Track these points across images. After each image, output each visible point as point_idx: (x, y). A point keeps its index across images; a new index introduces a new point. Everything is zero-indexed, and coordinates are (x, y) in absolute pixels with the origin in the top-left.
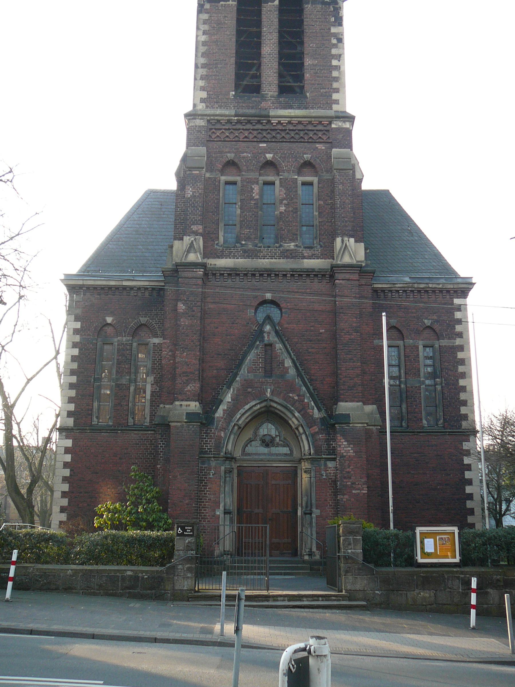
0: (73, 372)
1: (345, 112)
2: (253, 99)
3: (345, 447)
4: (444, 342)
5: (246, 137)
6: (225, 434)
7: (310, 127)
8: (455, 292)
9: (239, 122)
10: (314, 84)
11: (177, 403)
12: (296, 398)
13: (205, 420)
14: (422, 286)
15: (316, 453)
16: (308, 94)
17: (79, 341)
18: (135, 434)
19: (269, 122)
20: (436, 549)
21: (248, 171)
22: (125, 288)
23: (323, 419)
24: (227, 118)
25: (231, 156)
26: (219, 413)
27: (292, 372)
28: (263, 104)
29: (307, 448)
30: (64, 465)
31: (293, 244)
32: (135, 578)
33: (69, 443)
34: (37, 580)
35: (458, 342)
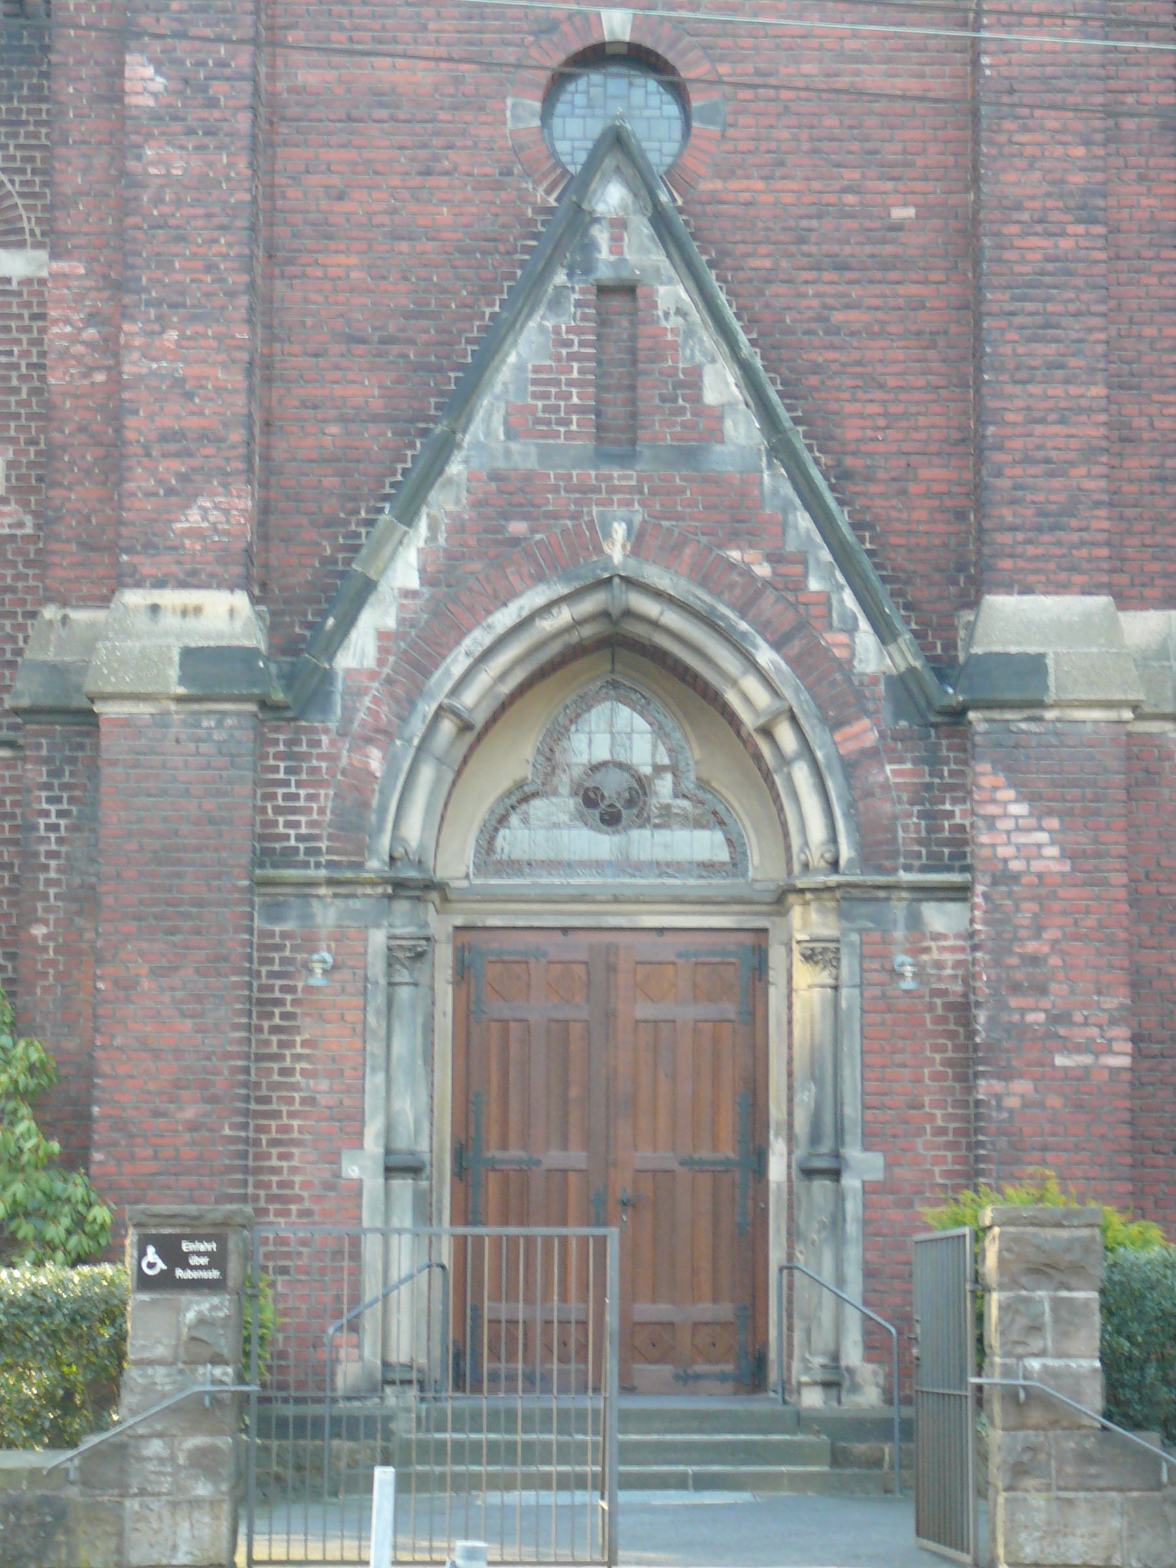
3: (1014, 829)
12: (763, 570)
15: (868, 856)
23: (902, 686)
26: (359, 651)
27: (743, 431)
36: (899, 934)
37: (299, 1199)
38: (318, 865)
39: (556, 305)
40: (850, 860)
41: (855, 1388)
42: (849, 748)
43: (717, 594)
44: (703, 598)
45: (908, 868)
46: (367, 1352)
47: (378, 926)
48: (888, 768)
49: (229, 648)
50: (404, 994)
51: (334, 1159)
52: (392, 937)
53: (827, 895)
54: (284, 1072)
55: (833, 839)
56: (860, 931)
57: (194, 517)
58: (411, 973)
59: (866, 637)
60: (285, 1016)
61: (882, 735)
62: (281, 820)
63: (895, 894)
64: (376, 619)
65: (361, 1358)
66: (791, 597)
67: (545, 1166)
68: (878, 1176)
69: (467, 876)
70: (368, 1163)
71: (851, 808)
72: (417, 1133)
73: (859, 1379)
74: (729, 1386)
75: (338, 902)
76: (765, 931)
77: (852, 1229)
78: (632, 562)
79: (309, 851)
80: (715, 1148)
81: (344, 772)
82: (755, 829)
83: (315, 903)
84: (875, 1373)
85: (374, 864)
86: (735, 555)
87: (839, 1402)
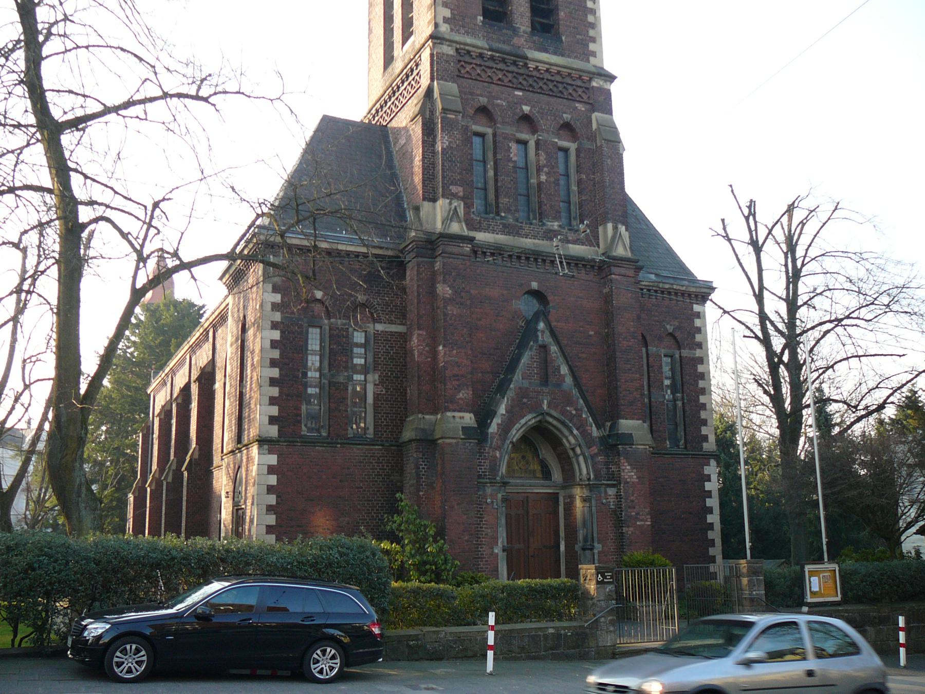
0: (273, 363)
1: (603, 69)
2: (504, 31)
3: (629, 473)
4: (685, 353)
5: (499, 79)
6: (501, 454)
7: (569, 81)
8: (696, 296)
9: (492, 58)
10: (569, 26)
11: (449, 414)
12: (574, 412)
13: (478, 433)
14: (667, 286)
15: (596, 478)
16: (563, 38)
17: (279, 320)
18: (358, 449)
19: (526, 64)
20: (820, 588)
21: (503, 123)
22: (339, 253)
23: (602, 438)
24: (479, 51)
25: (483, 100)
26: (493, 428)
27: (569, 380)
28: (515, 40)
29: (584, 471)
30: (268, 490)
31: (556, 223)
32: (558, 636)
33: (273, 460)
34: (452, 647)
35: (698, 353)
39: (531, 349)
49: (214, 399)
57: (461, 395)
59: (594, 428)
64: (497, 421)
71: (593, 466)
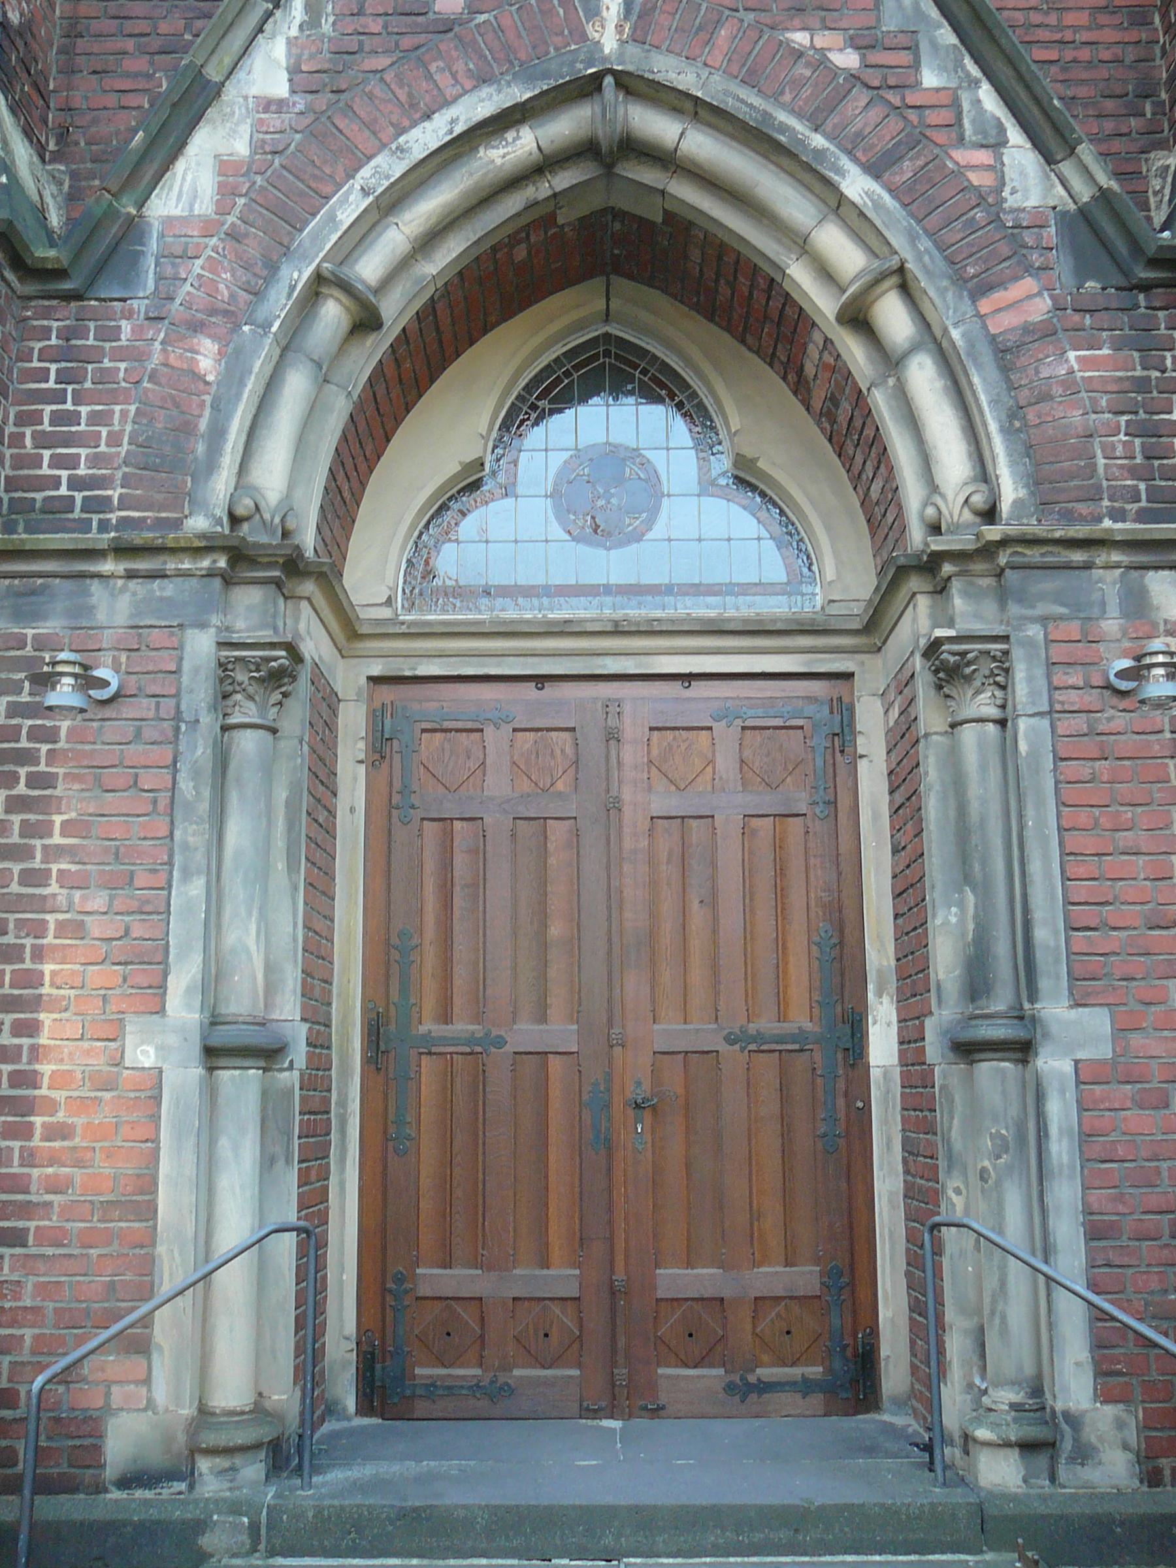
12: (848, 60)
15: (1044, 489)
36: (1111, 625)
37: (51, 1107)
38: (104, 526)
40: (1017, 503)
41: (1083, 1454)
42: (1003, 323)
43: (775, 96)
44: (747, 101)
45: (1118, 515)
46: (161, 1392)
47: (203, 626)
48: (1072, 355)
50: (248, 743)
51: (116, 1035)
52: (222, 645)
53: (979, 566)
54: (28, 877)
55: (983, 474)
56: (1044, 620)
58: (263, 709)
59: (1020, 156)
60: (35, 781)
61: (1059, 308)
62: (47, 454)
63: (1101, 557)
65: (150, 1405)
66: (895, 99)
67: (509, 1048)
68: (1105, 1051)
69: (389, 602)
70: (172, 1040)
72: (271, 989)
73: (1090, 1435)
74: (817, 1400)
75: (133, 584)
76: (849, 676)
77: (1061, 1149)
78: (633, 50)
79: (90, 505)
80: (782, 1017)
81: (152, 378)
82: (828, 529)
83: (95, 586)
84: (1120, 1425)
85: (198, 523)
86: (800, 38)
87: (1053, 1478)
